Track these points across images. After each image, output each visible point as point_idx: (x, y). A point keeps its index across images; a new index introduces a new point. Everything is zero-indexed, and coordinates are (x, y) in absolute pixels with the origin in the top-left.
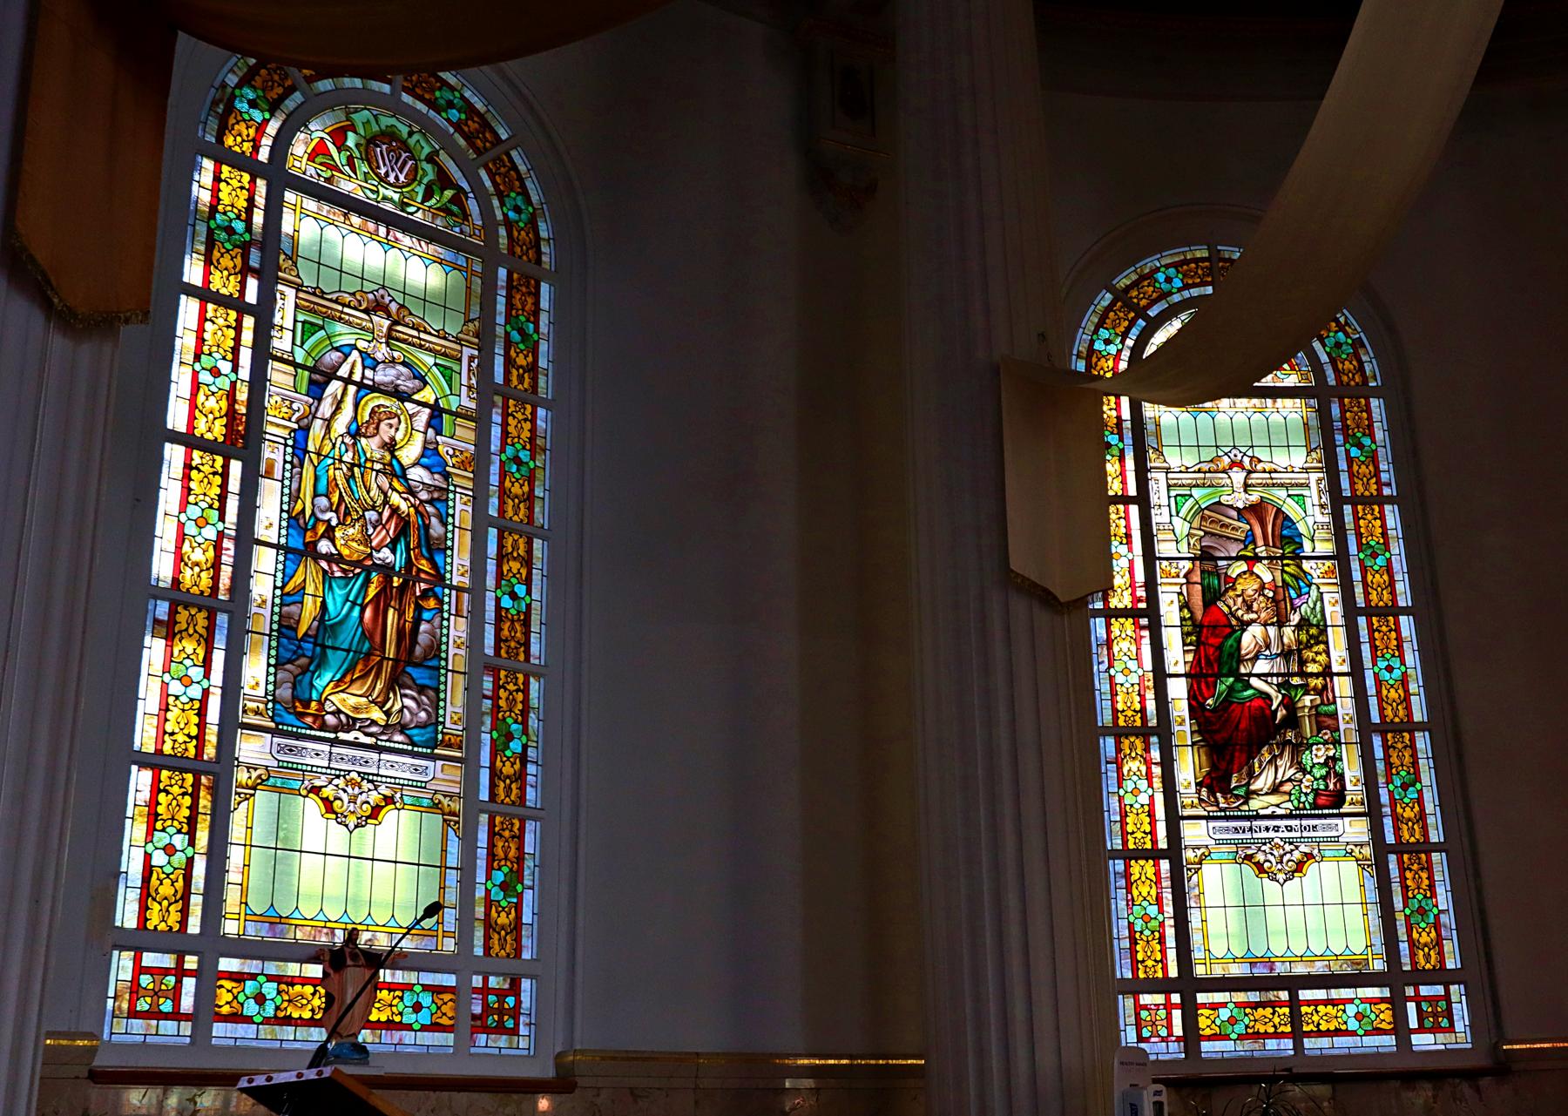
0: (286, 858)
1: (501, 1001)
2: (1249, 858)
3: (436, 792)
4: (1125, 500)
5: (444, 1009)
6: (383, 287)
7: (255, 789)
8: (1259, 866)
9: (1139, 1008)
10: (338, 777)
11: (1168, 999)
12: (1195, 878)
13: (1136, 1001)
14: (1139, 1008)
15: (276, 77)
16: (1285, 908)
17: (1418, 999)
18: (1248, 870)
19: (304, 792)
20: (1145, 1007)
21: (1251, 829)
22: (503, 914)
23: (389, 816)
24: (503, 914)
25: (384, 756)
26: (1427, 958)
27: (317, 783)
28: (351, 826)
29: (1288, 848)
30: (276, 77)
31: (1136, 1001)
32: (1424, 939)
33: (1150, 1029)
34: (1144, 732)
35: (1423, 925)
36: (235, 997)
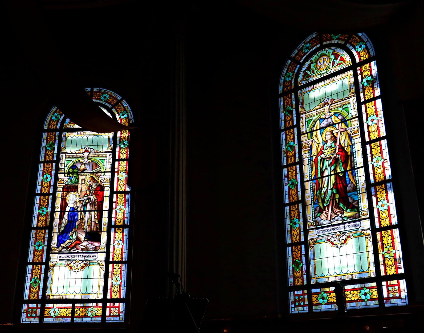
0: (363, 255)
1: (299, 298)
2: (68, 265)
3: (362, 230)
4: (120, 160)
5: (316, 299)
6: (326, 98)
7: (314, 244)
8: (71, 268)
9: (110, 316)
10: (334, 235)
11: (108, 307)
12: (51, 271)
13: (108, 316)
14: (110, 316)
15: (354, 39)
16: (77, 279)
17: (37, 308)
18: (67, 268)
19: (326, 242)
20: (110, 314)
21: (85, 256)
22: (298, 273)
23: (349, 241)
24: (298, 273)
25: (345, 225)
26: (296, 239)
27: (329, 238)
28: (339, 247)
29: (80, 262)
30: (354, 39)
31: (108, 316)
32: (34, 290)
33: (116, 312)
34: (116, 226)
35: (35, 286)
36: (372, 293)
